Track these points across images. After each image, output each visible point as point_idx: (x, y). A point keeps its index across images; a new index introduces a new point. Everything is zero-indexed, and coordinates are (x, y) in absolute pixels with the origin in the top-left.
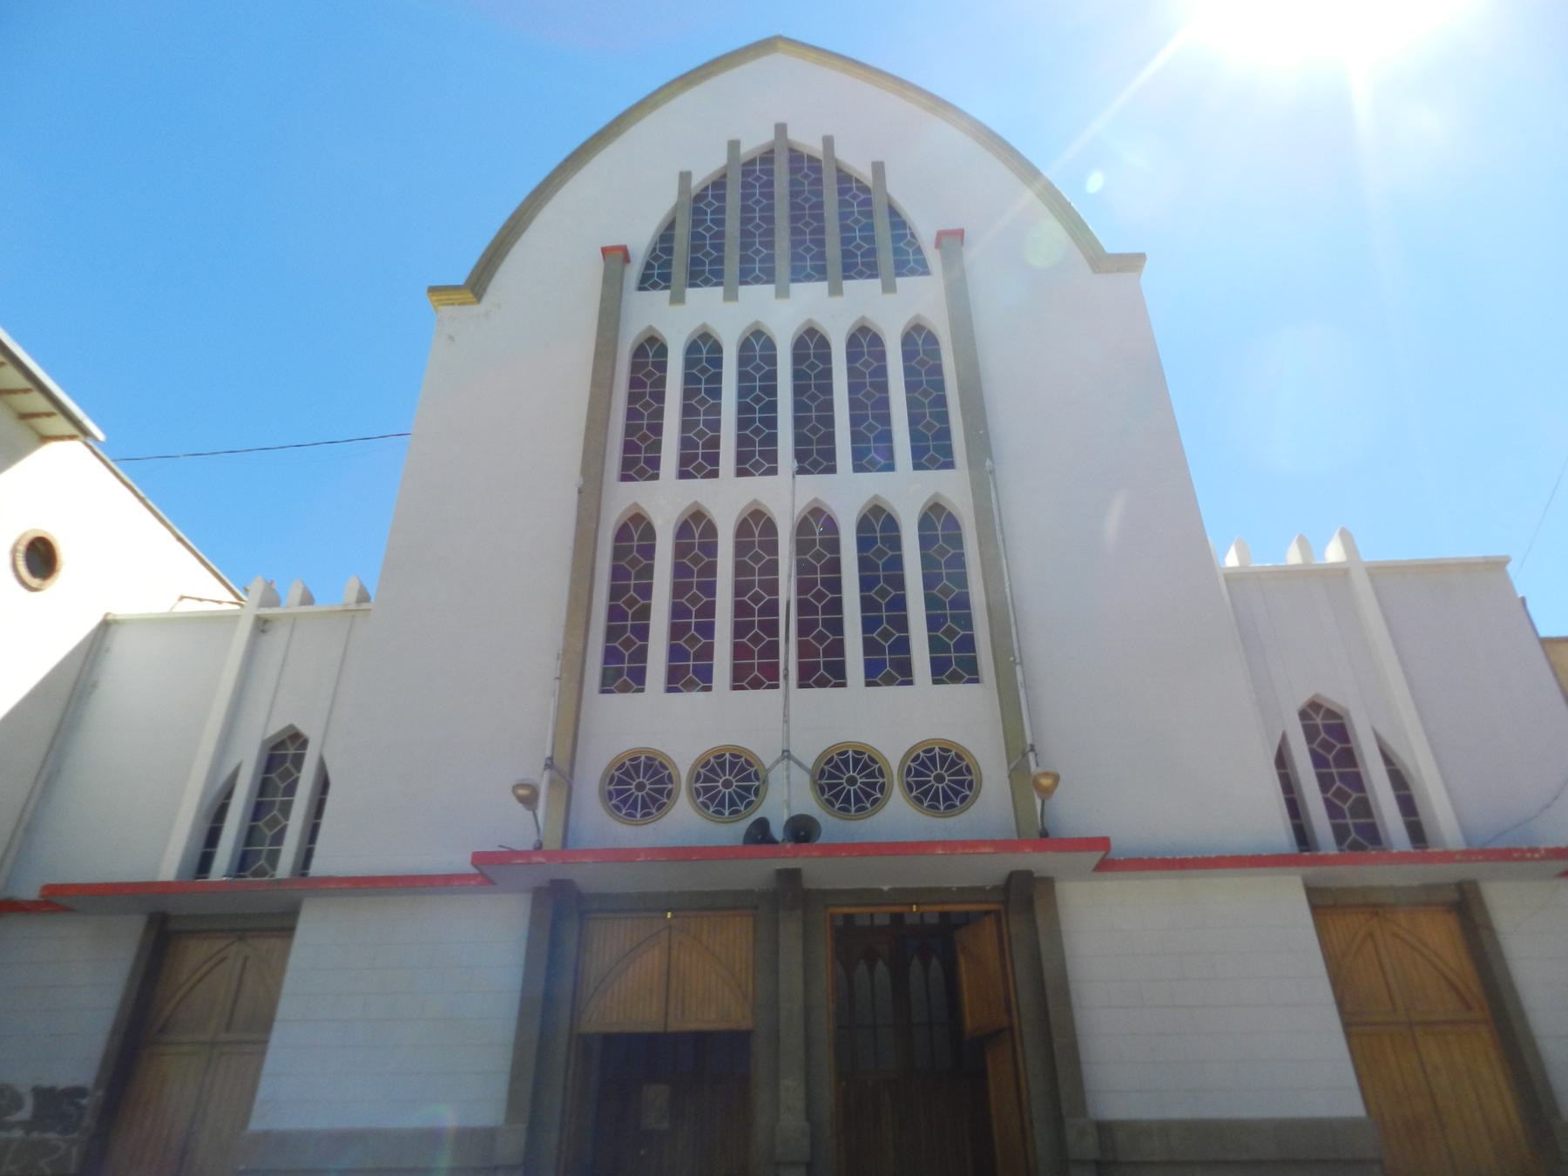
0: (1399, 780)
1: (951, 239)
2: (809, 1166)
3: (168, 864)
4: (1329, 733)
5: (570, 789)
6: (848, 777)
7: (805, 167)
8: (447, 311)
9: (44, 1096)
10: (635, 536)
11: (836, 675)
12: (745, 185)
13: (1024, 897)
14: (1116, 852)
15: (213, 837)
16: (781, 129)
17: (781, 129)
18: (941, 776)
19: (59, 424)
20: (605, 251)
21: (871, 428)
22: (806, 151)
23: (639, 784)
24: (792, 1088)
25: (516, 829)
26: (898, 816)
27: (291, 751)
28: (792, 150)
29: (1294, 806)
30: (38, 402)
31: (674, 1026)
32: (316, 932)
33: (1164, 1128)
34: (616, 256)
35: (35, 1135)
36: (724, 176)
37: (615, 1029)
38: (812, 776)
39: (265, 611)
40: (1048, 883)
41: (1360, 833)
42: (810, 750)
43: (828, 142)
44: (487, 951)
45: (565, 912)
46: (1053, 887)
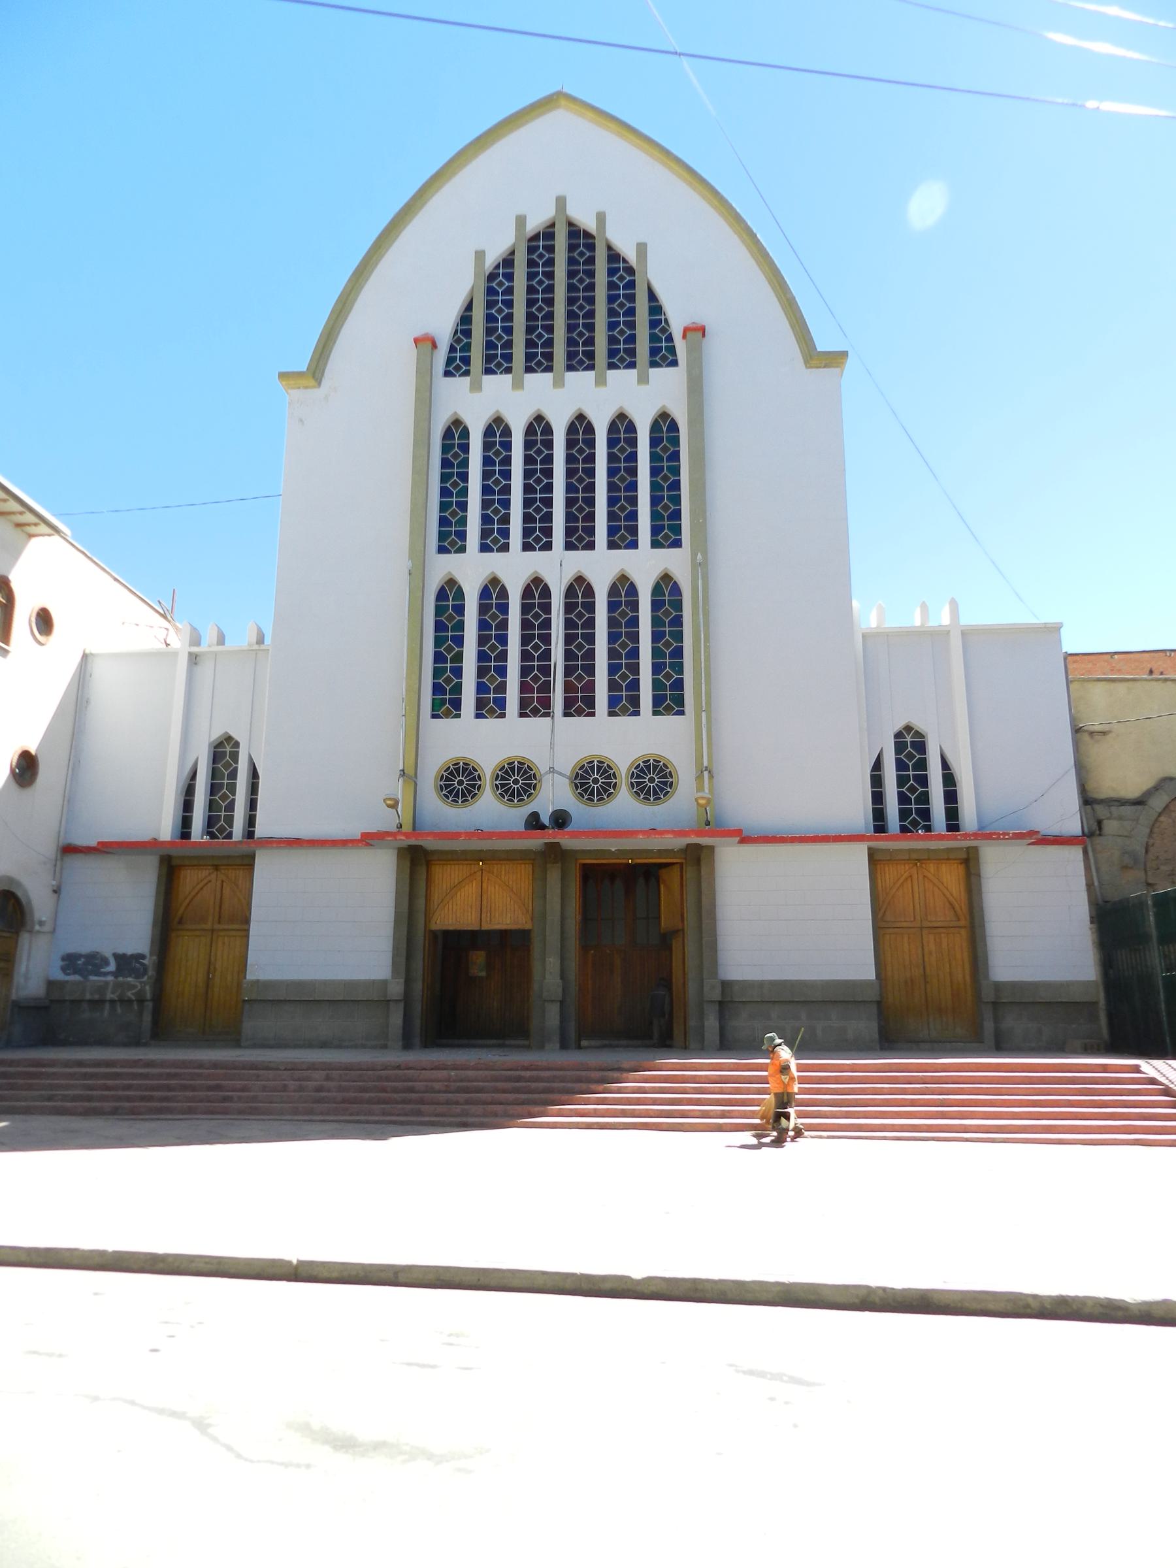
0: (949, 779)
1: (697, 331)
2: (562, 1002)
3: (165, 828)
4: (911, 747)
5: (416, 784)
6: (593, 780)
7: (581, 241)
8: (296, 394)
9: (121, 959)
10: (449, 597)
11: (588, 707)
12: (531, 263)
13: (697, 858)
14: (745, 834)
15: (188, 806)
16: (561, 202)
17: (561, 202)
18: (653, 779)
19: (43, 528)
20: (416, 341)
21: (623, 508)
22: (582, 227)
23: (459, 781)
24: (553, 962)
25: (385, 821)
26: (624, 807)
27: (228, 749)
28: (570, 224)
29: (878, 797)
30: (29, 518)
31: (485, 927)
32: (269, 876)
33: (761, 984)
34: (426, 342)
35: (121, 979)
36: (513, 253)
37: (451, 928)
38: (570, 779)
39: (195, 649)
40: (711, 849)
41: (916, 813)
42: (568, 762)
43: (601, 218)
44: (375, 881)
45: (418, 860)
46: (713, 852)
